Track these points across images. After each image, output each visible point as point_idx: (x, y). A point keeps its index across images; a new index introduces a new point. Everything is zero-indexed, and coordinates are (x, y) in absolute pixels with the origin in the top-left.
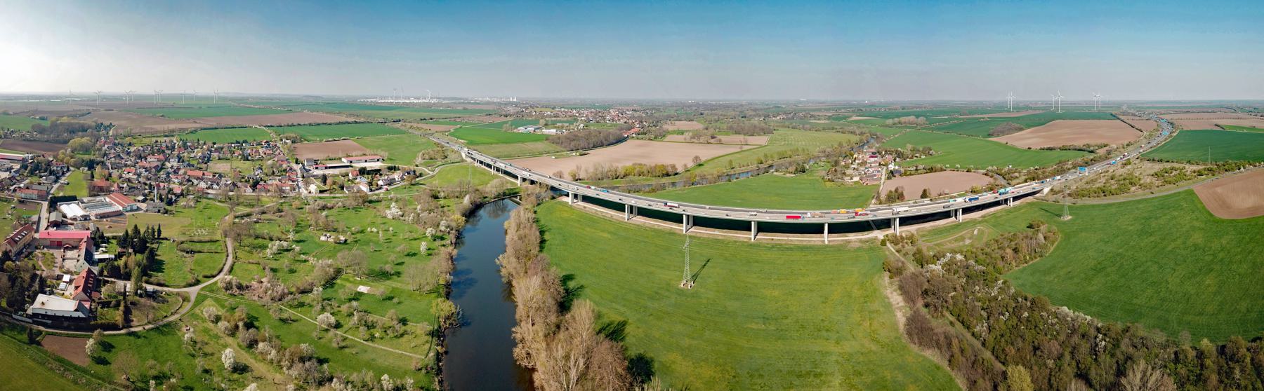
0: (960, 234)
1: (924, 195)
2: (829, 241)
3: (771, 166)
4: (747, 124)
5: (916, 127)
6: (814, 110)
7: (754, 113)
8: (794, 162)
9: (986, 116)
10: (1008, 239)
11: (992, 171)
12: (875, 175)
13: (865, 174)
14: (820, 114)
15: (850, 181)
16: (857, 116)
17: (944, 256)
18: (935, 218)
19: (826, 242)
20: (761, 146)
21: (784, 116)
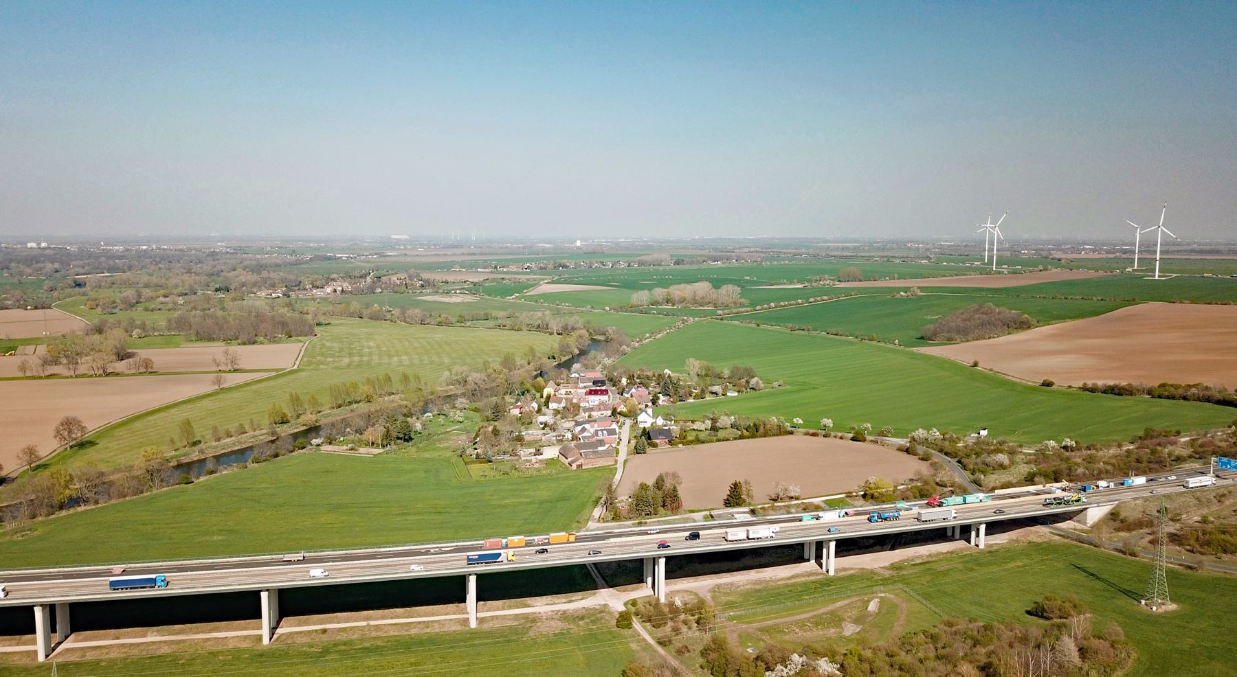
0: (830, 608)
1: (735, 498)
2: (481, 621)
3: (313, 430)
4: (234, 308)
5: (714, 313)
6: (431, 267)
7: (255, 277)
8: (380, 413)
9: (914, 283)
10: (965, 635)
11: (925, 442)
12: (602, 443)
13: (575, 438)
14: (450, 278)
15: (533, 459)
16: (553, 282)
17: (784, 661)
18: (763, 560)
19: (473, 624)
20: (281, 374)
21: (346, 286)
